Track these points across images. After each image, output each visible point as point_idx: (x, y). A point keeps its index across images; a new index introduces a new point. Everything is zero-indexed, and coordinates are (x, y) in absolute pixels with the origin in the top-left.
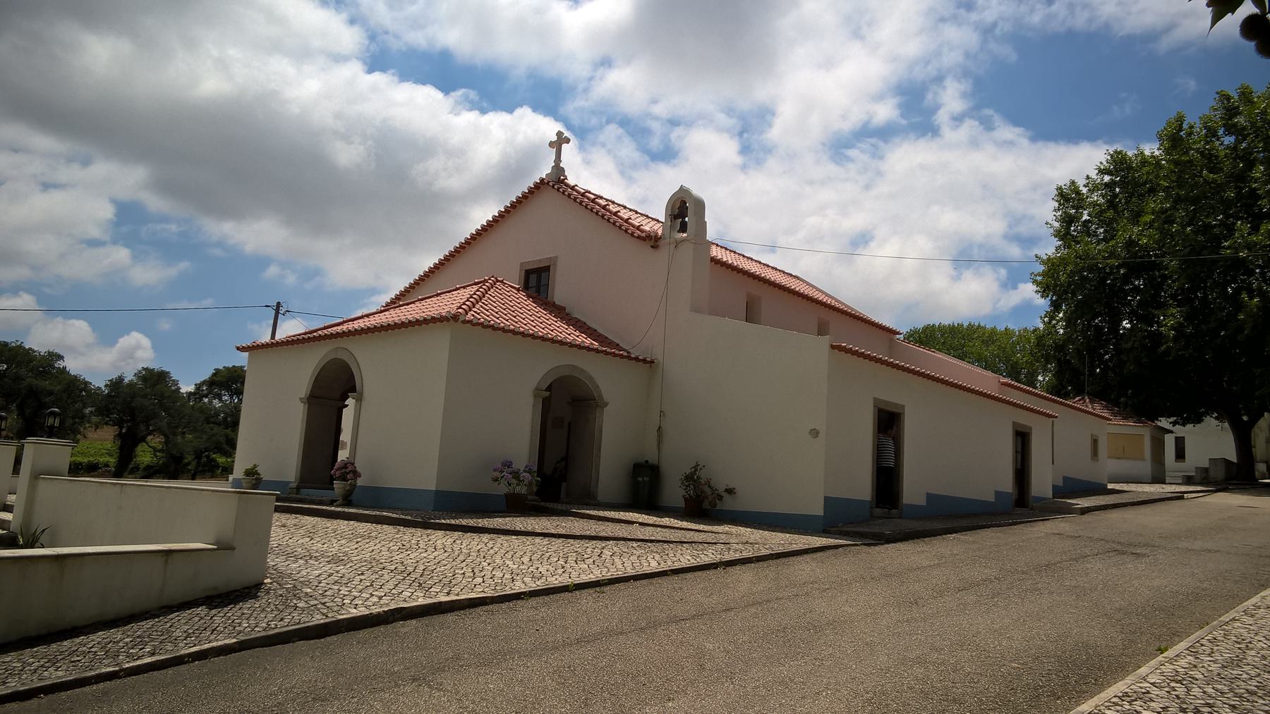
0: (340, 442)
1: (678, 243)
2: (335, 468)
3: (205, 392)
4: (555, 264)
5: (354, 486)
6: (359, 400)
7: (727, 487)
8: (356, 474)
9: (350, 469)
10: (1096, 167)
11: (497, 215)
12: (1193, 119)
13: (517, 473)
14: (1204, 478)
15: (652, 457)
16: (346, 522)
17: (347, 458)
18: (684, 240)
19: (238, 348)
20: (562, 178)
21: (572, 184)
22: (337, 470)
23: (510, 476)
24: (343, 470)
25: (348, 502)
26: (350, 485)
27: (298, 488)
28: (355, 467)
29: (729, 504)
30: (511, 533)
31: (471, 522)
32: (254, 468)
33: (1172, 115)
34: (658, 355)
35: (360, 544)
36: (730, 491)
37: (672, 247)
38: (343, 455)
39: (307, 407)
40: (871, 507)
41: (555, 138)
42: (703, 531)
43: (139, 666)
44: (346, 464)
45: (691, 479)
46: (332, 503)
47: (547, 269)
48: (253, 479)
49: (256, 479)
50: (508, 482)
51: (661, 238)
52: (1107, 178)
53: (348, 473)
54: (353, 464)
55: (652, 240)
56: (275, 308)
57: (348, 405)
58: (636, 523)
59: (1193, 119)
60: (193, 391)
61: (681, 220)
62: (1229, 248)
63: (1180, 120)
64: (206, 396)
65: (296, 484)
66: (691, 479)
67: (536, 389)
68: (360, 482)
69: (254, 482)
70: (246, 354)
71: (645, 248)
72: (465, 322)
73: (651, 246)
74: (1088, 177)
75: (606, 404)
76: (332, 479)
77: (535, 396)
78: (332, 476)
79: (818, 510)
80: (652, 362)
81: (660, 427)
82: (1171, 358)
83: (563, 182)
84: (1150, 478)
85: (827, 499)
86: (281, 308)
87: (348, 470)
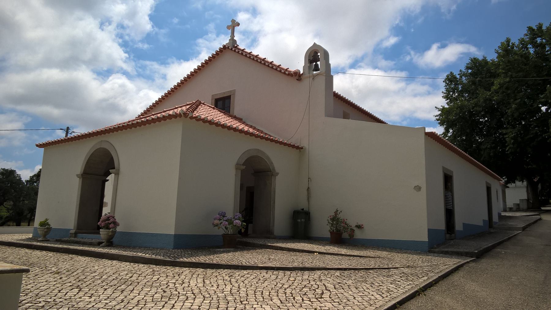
0: (104, 203)
1: (314, 77)
2: (101, 220)
3: (35, 180)
4: (234, 94)
5: (114, 232)
6: (117, 174)
7: (356, 224)
8: (116, 224)
9: (112, 220)
10: (465, 66)
11: (193, 71)
12: (515, 40)
13: (231, 220)
14: (518, 208)
15: (303, 204)
16: (110, 261)
17: (109, 213)
18: (317, 75)
19: (37, 146)
20: (236, 45)
21: (242, 49)
22: (102, 222)
23: (227, 223)
24: (107, 222)
25: (110, 244)
26: (112, 232)
27: (76, 234)
28: (115, 220)
29: (358, 235)
30: (240, 268)
31: (202, 259)
32: (46, 221)
33: (503, 40)
34: (304, 144)
35: (125, 293)
36: (359, 227)
37: (311, 79)
38: (106, 211)
39: (81, 180)
40: (446, 234)
41: (231, 24)
42: (363, 257)
43: (60, 244)
44: (109, 218)
45: (335, 219)
46: (99, 244)
47: (229, 98)
48: (45, 228)
49: (47, 228)
50: (225, 227)
51: (302, 74)
52: (470, 71)
53: (110, 224)
54: (113, 217)
55: (297, 75)
56: (66, 130)
57: (108, 180)
58: (316, 252)
59: (515, 40)
60: (29, 180)
61: (314, 63)
62: (543, 98)
63: (508, 41)
64: (36, 182)
65: (74, 231)
66: (335, 219)
67: (237, 164)
68: (118, 229)
69: (46, 230)
70: (42, 149)
71: (293, 81)
72: (192, 118)
73: (297, 80)
74: (461, 71)
75: (278, 174)
76: (99, 228)
77: (236, 169)
78: (98, 226)
79: (425, 238)
80: (302, 148)
81: (308, 188)
82: (508, 152)
83: (236, 47)
84: (503, 209)
85: (429, 231)
86: (69, 130)
87: (110, 222)
